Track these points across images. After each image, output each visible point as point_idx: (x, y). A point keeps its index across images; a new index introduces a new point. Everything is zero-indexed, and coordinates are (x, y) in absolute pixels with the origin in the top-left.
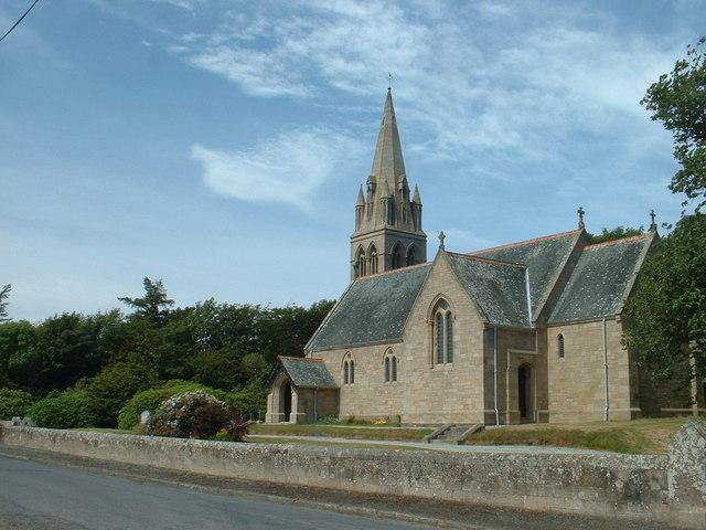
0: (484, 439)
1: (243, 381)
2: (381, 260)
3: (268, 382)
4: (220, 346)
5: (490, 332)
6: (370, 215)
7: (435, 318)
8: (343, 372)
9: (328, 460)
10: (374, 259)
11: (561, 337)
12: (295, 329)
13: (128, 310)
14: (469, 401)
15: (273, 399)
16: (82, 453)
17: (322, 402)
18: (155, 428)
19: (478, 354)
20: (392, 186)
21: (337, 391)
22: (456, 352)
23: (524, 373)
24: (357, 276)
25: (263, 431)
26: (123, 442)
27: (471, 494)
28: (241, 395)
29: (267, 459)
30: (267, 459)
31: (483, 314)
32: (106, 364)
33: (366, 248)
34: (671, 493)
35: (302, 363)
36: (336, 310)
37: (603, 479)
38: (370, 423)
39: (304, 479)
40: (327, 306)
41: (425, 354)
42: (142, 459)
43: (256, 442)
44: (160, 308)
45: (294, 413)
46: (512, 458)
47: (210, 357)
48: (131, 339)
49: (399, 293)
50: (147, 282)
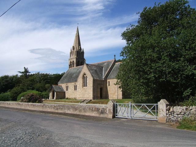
0: (91, 103)
1: (45, 90)
2: (75, 64)
3: (50, 91)
4: (161, 58)
5: (94, 81)
6: (73, 54)
7: (83, 77)
8: (66, 88)
9: (53, 106)
10: (73, 64)
11: (109, 82)
12: (57, 78)
13: (20, 74)
14: (90, 95)
15: (51, 94)
16: (7, 106)
17: (61, 96)
18: (22, 101)
19: (92, 85)
20: (78, 48)
21: (65, 92)
22: (87, 84)
23: (101, 89)
24: (70, 68)
25: (48, 101)
26: (15, 104)
27: (77, 112)
28: (45, 93)
29: (43, 106)
30: (43, 106)
31: (93, 77)
32: (15, 87)
33: (72, 62)
34: (108, 112)
35: (57, 86)
36: (65, 75)
37: (97, 110)
38: (71, 99)
39: (49, 110)
40: (64, 73)
41: (82, 85)
42: (19, 107)
43: (46, 102)
44: (28, 74)
45: (55, 97)
46: (84, 106)
47: (38, 85)
48: (20, 81)
49: (78, 71)
50: (25, 68)
